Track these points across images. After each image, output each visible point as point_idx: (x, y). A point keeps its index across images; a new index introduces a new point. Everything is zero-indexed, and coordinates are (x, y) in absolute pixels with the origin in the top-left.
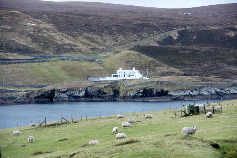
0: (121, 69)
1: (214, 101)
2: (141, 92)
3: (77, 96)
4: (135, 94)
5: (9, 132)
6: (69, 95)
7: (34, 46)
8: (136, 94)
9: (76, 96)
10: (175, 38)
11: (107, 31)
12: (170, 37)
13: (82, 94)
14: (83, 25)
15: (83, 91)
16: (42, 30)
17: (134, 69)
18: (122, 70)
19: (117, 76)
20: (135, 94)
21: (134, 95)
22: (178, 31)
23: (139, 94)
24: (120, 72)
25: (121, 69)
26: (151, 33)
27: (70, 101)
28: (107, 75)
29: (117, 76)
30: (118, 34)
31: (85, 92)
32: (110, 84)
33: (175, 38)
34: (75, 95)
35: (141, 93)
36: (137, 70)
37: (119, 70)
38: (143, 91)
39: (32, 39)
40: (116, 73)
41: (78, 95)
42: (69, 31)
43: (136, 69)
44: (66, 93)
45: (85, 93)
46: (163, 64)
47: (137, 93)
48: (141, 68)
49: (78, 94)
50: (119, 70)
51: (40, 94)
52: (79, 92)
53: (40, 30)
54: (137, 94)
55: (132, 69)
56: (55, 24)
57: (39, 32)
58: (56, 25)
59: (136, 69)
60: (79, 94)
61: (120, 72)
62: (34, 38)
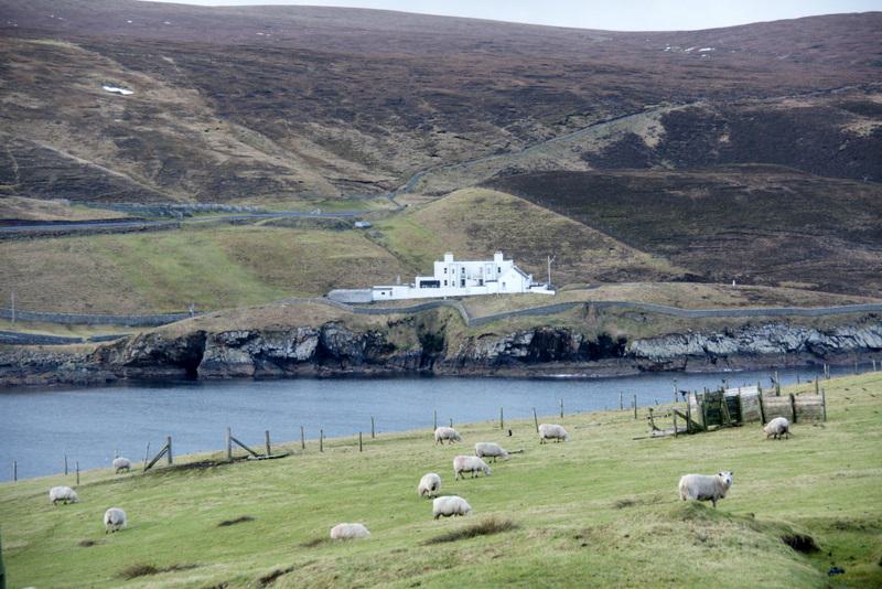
0: (449, 257)
1: (795, 377)
2: (523, 342)
3: (288, 358)
4: (502, 350)
5: (35, 492)
6: (257, 356)
7: (126, 172)
8: (506, 349)
9: (282, 358)
10: (651, 142)
11: (398, 114)
12: (633, 139)
13: (305, 350)
14: (309, 93)
15: (309, 341)
16: (155, 111)
17: (499, 257)
18: (455, 260)
19: (436, 284)
20: (502, 350)
21: (500, 353)
22: (663, 114)
23: (517, 350)
24: (447, 270)
25: (449, 257)
26: (560, 123)
27: (259, 378)
28: (399, 279)
29: (436, 284)
30: (438, 125)
31: (316, 342)
32: (411, 315)
33: (651, 142)
34: (279, 353)
35: (525, 345)
36: (508, 259)
37: (442, 260)
38: (533, 340)
39: (119, 144)
40: (432, 274)
41: (292, 355)
42: (257, 115)
43: (505, 259)
44: (244, 348)
45: (316, 348)
46: (606, 239)
47: (509, 346)
48: (525, 254)
49: (289, 350)
50: (442, 260)
51: (148, 350)
52: (295, 342)
53: (148, 113)
54: (508, 352)
55: (491, 257)
56: (204, 91)
57: (146, 119)
58: (209, 95)
59: (505, 259)
60: (294, 351)
61: (447, 270)
62: (126, 143)
